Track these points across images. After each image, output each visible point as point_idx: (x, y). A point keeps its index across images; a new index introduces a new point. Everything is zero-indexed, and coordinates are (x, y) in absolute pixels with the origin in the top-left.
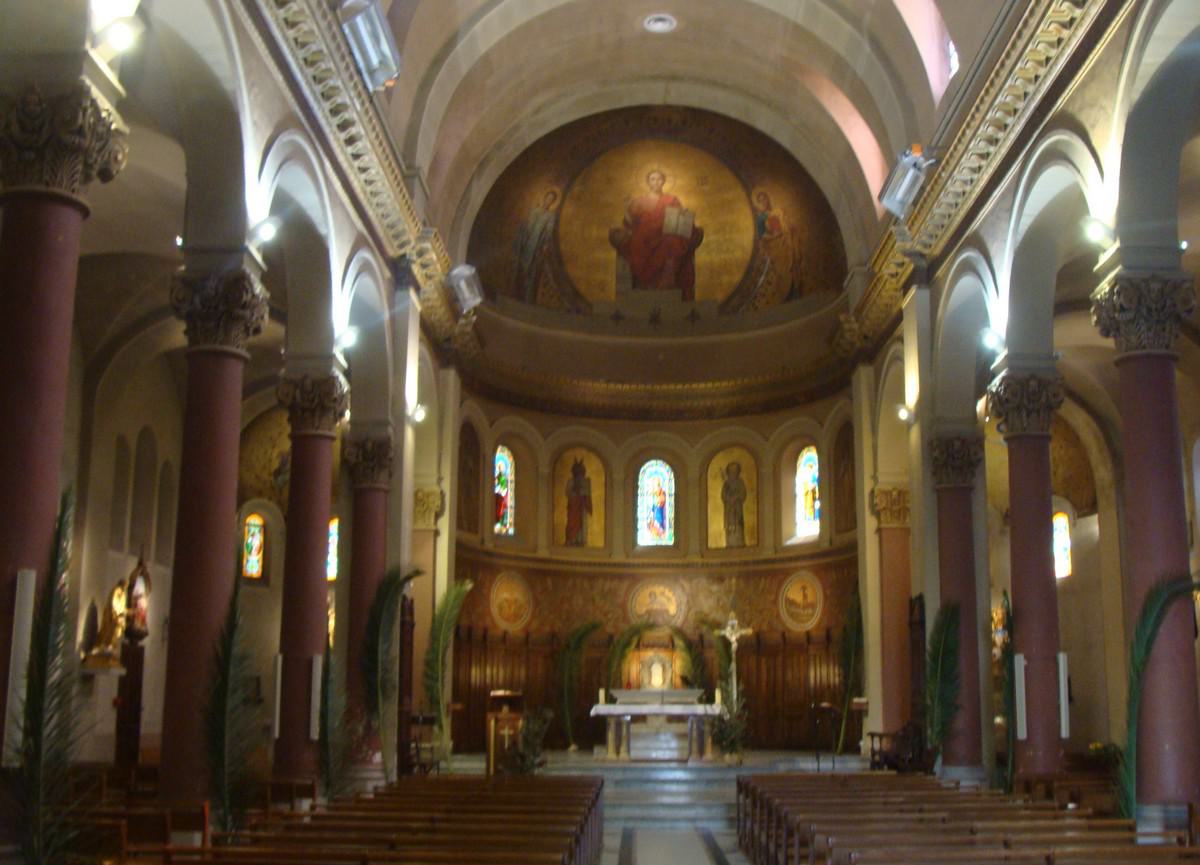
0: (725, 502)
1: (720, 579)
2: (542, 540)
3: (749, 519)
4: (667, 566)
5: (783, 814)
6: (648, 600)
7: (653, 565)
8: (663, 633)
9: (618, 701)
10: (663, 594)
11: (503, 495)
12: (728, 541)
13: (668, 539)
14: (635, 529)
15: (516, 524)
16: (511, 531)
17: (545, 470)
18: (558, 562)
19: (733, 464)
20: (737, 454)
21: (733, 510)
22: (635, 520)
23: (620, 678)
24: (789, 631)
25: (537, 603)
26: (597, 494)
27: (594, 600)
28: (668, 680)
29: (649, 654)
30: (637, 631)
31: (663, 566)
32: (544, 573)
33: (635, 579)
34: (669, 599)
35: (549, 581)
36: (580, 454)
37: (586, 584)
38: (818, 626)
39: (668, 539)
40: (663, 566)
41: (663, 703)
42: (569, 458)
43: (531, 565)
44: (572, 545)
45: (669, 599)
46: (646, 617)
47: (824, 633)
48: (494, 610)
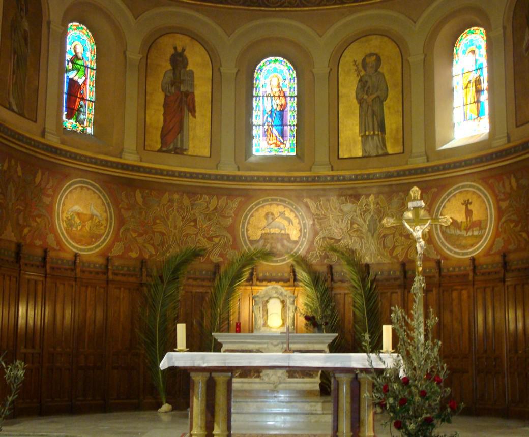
0: (360, 101)
1: (356, 197)
2: (130, 142)
3: (392, 122)
4: (290, 180)
5: (333, 295)
6: (264, 223)
7: (270, 179)
8: (282, 264)
9: (225, 347)
10: (282, 214)
11: (81, 81)
12: (364, 151)
13: (288, 149)
14: (250, 137)
15: (96, 124)
16: (90, 130)
17: (134, 55)
18: (149, 171)
19: (371, 55)
20: (375, 44)
21: (370, 112)
22: (249, 127)
23: (228, 319)
24: (446, 258)
25: (121, 221)
26: (202, 91)
27: (195, 221)
28: (289, 322)
29: (262, 290)
30: (249, 260)
31: (283, 180)
32: (130, 184)
33: (247, 196)
34: (290, 221)
35: (138, 194)
36: (181, 41)
37: (186, 201)
38: (488, 252)
39: (288, 149)
40: (283, 180)
41: (288, 350)
42: (168, 46)
43: (119, 173)
44: (168, 152)
45: (290, 221)
46: (261, 243)
47: (498, 258)
48: (61, 226)
